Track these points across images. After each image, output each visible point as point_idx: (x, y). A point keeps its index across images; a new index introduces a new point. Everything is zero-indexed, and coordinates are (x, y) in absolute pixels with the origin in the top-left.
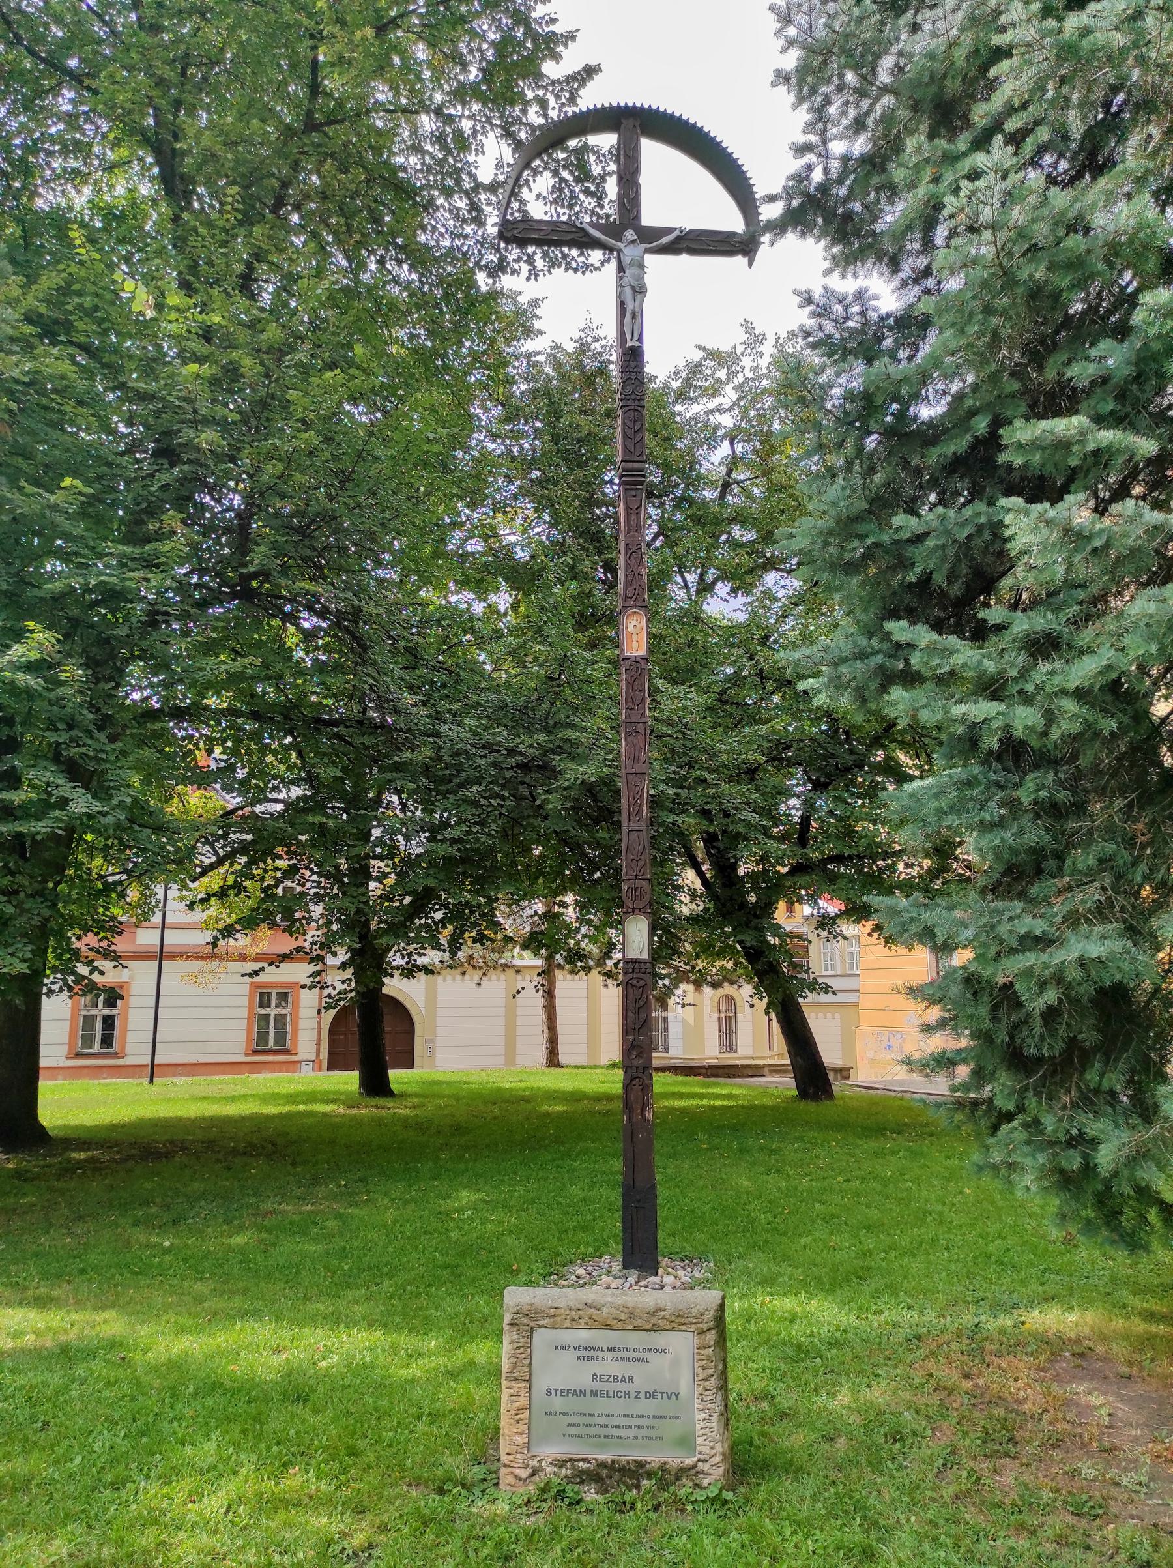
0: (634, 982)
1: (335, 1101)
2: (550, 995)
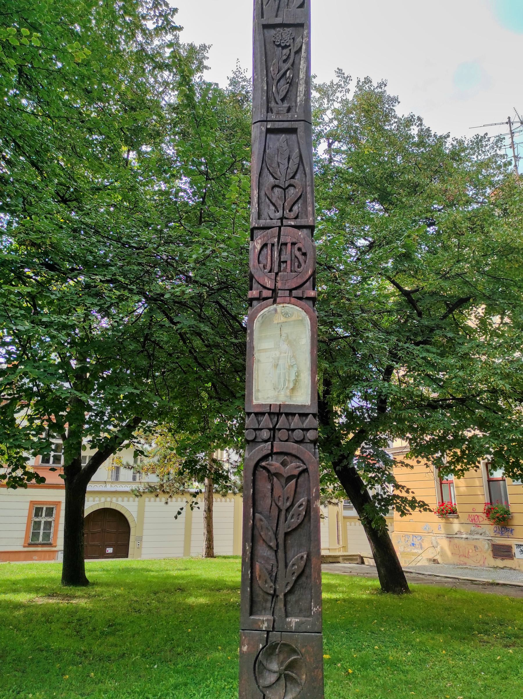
0: (274, 464)
1: (37, 590)
2: (209, 510)
